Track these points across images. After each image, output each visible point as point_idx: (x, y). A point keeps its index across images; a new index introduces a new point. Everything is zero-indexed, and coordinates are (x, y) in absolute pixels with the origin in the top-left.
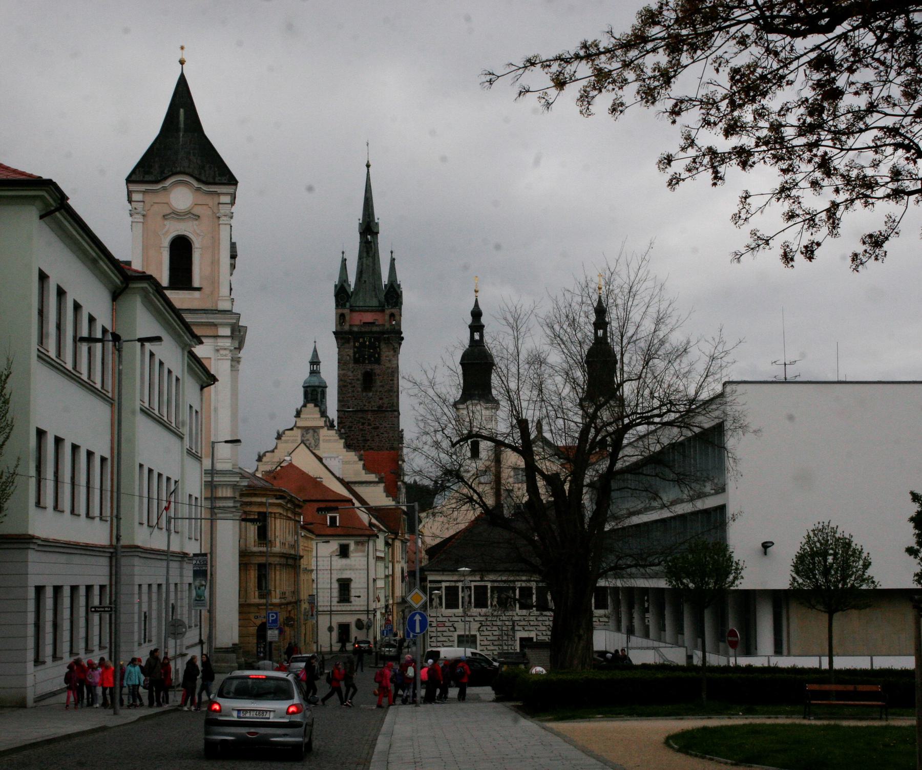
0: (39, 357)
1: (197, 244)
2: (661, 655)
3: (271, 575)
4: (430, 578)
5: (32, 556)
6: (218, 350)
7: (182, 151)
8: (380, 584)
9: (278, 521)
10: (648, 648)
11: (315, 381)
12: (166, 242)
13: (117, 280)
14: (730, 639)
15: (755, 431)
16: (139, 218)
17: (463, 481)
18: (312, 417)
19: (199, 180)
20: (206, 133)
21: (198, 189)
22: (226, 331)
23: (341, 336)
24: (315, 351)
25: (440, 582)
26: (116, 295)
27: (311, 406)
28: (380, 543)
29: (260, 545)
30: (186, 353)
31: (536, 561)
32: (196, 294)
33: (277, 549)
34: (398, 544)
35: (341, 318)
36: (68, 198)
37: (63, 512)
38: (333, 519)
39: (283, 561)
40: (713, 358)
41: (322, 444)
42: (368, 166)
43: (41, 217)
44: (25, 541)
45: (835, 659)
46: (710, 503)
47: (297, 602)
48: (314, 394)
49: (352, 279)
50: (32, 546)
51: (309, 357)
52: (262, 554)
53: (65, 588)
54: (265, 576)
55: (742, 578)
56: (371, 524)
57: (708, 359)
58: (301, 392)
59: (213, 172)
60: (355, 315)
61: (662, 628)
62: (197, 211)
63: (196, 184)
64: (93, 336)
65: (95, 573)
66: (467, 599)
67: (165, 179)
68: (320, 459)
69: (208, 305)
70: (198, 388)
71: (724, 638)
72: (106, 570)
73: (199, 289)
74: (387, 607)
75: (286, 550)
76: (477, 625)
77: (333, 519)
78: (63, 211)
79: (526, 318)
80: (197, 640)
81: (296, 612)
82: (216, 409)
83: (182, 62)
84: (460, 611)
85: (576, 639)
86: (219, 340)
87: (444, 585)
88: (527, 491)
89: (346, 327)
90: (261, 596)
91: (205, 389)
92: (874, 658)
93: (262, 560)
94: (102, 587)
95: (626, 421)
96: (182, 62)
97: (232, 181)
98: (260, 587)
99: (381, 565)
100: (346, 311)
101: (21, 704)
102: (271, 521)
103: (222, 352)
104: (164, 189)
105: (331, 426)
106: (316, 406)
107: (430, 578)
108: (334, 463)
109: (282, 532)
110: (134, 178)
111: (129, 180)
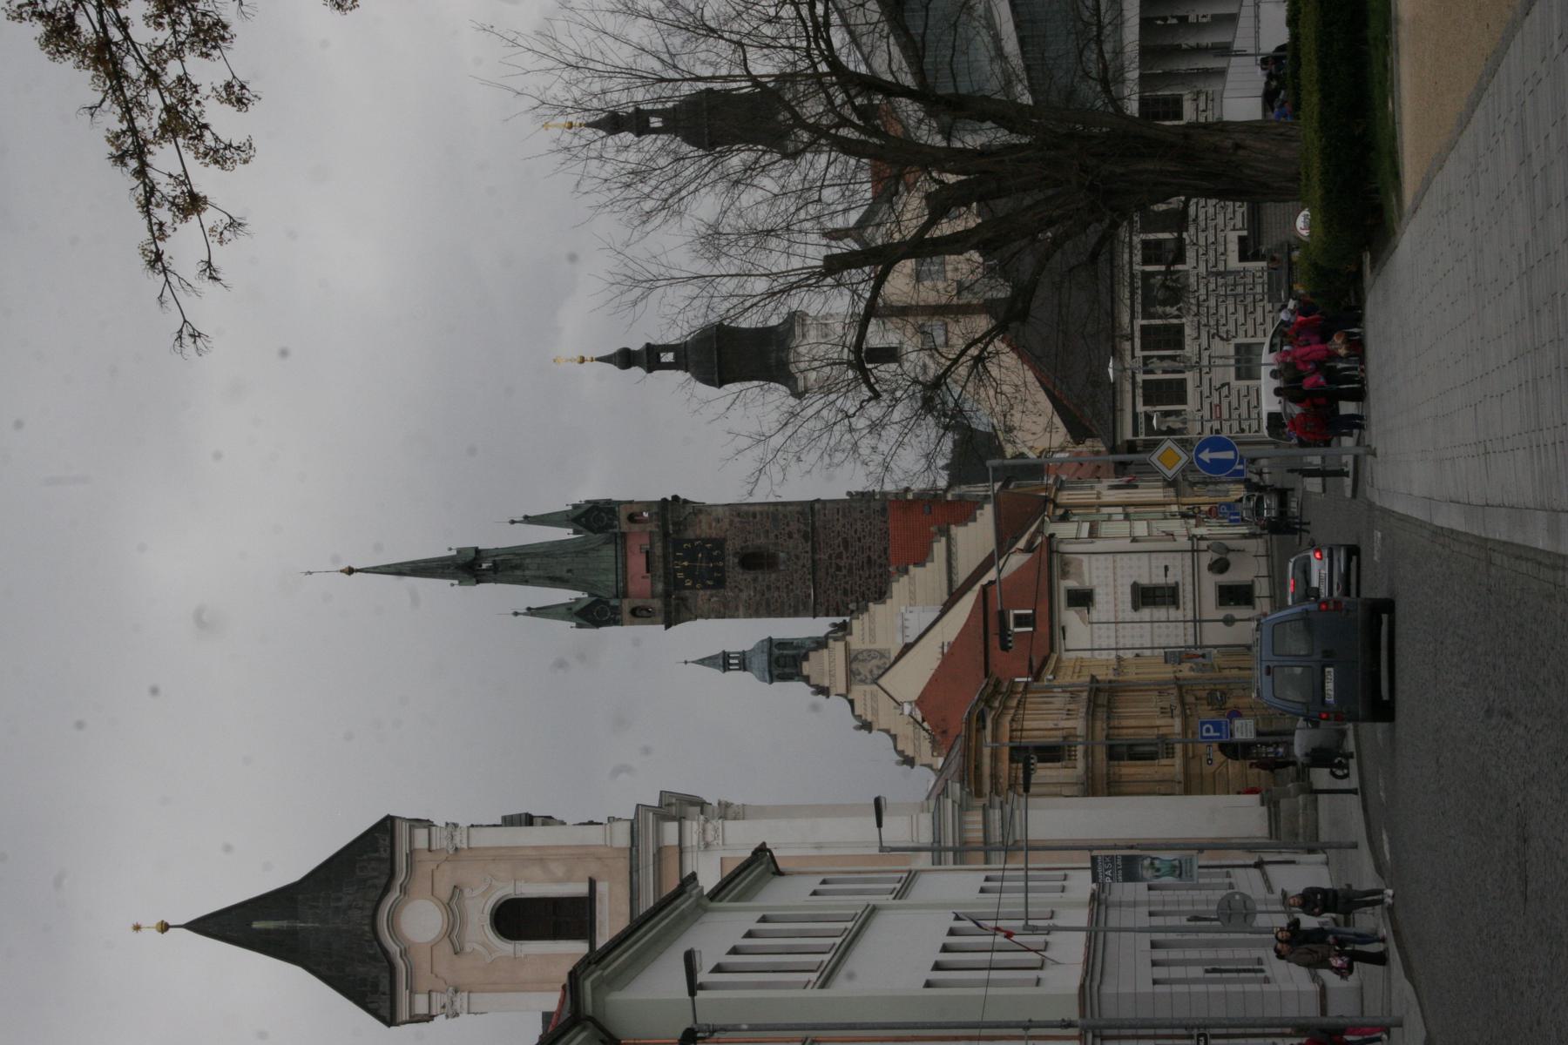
1: (507, 890)
4: (1129, 436)
6: (707, 845)
8: (1141, 529)
9: (1027, 725)
10: (1257, 16)
11: (761, 661)
12: (507, 947)
18: (829, 664)
19: (387, 889)
21: (404, 890)
22: (671, 829)
24: (702, 662)
25: (1135, 416)
27: (806, 668)
28: (1063, 530)
29: (1071, 757)
32: (602, 887)
33: (1078, 725)
34: (1065, 497)
35: (640, 614)
38: (1020, 621)
41: (879, 645)
42: (350, 571)
47: (1180, 685)
48: (784, 662)
49: (563, 596)
51: (715, 673)
56: (1029, 548)
59: (370, 863)
62: (444, 891)
63: (395, 894)
66: (1166, 364)
67: (385, 952)
68: (908, 647)
69: (623, 865)
70: (778, 879)
73: (592, 884)
74: (1184, 516)
77: (1020, 621)
79: (630, 264)
80: (1256, 872)
82: (819, 846)
83: (164, 927)
84: (1190, 377)
85: (1241, 152)
87: (1141, 408)
89: (657, 604)
90: (1170, 754)
91: (781, 866)
93: (1101, 754)
96: (164, 927)
97: (387, 826)
98: (1152, 756)
99: (1105, 529)
100: (626, 605)
104: (404, 953)
105: (844, 628)
106: (806, 657)
108: (916, 622)
109: (1048, 717)
110: (385, 1013)
111: (390, 1020)
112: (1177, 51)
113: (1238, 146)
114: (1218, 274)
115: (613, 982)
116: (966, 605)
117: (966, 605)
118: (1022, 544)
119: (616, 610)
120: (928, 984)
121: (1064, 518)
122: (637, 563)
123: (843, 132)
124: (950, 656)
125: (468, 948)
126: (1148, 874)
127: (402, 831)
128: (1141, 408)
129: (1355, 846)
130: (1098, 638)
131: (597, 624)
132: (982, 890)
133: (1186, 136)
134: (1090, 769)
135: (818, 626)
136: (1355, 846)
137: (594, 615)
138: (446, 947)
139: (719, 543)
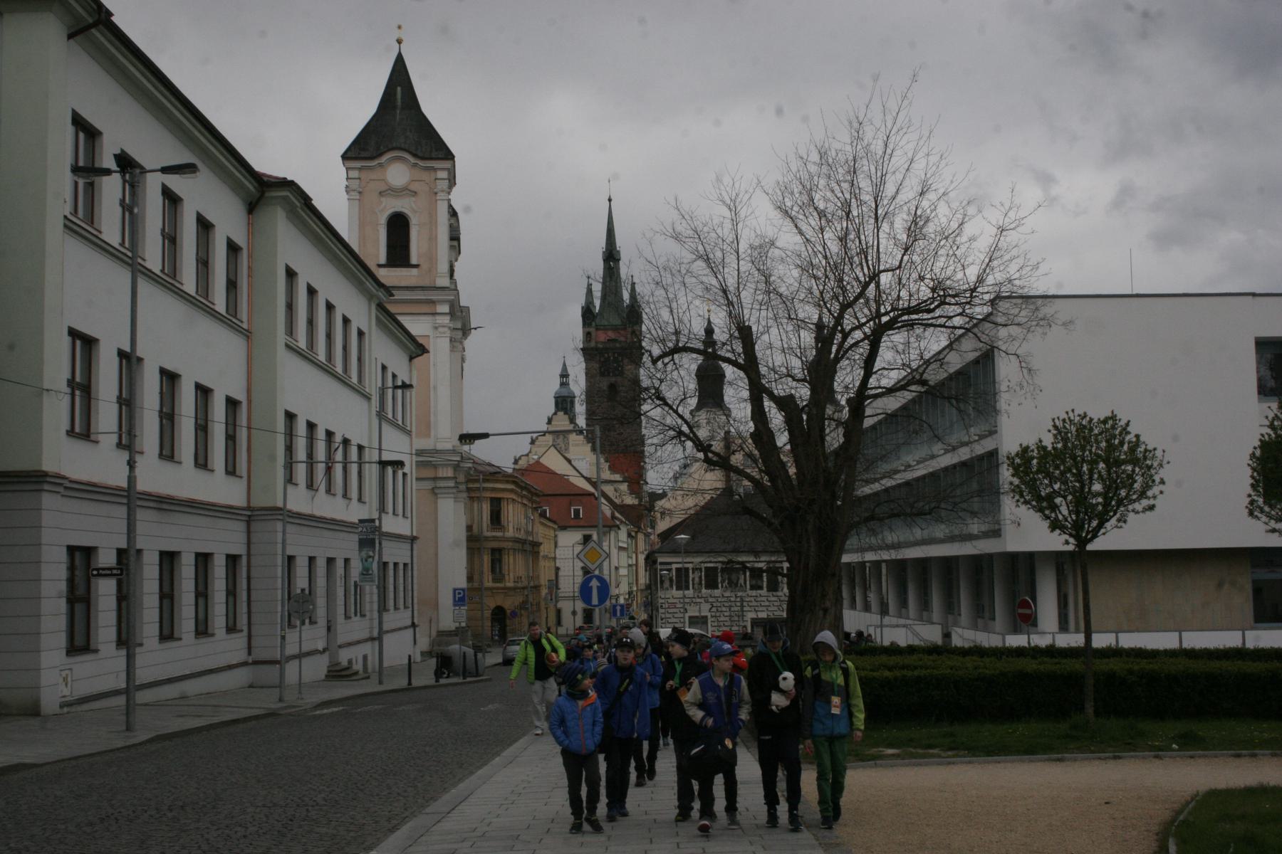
0: (65, 226)
1: (414, 221)
2: (916, 634)
3: (505, 558)
4: (660, 560)
5: (50, 501)
6: (436, 328)
7: (399, 129)
8: (623, 572)
9: (511, 507)
10: (897, 626)
11: (564, 392)
12: (383, 220)
13: (251, 187)
14: (1020, 611)
15: (1064, 324)
16: (355, 195)
17: (666, 404)
18: (562, 422)
19: (415, 155)
20: (424, 110)
21: (415, 165)
22: (446, 309)
23: (588, 353)
24: (564, 365)
25: (670, 563)
26: (252, 208)
27: (561, 413)
28: (623, 534)
29: (493, 530)
30: (374, 307)
31: (766, 513)
32: (414, 271)
33: (510, 533)
34: (641, 536)
35: (588, 335)
36: (111, 15)
37: (180, 463)
38: (577, 512)
39: (517, 546)
40: (1002, 230)
41: (571, 448)
42: (610, 200)
43: (70, 37)
44: (36, 479)
45: (1095, 636)
46: (980, 449)
47: (537, 588)
48: (564, 403)
49: (597, 303)
50: (46, 487)
51: (559, 371)
52: (495, 539)
53: (184, 555)
54: (500, 561)
55: (1162, 482)
56: (613, 517)
57: (994, 230)
58: (553, 401)
59: (430, 148)
60: (600, 333)
61: (903, 603)
62: (414, 187)
63: (412, 160)
64: (97, 165)
65: (224, 540)
66: (697, 580)
67: (381, 155)
68: (569, 461)
69: (426, 283)
70: (407, 359)
71: (982, 613)
72: (242, 538)
73: (417, 266)
74: (630, 593)
75: (522, 535)
76: (708, 606)
77: (577, 512)
78: (101, 27)
79: (747, 197)
80: (409, 623)
81: (536, 597)
82: (435, 388)
83: (399, 42)
84: (690, 593)
85: (821, 613)
86: (438, 317)
87: (674, 566)
88: (752, 419)
89: (593, 344)
90: (495, 580)
91: (416, 361)
92: (1184, 634)
93: (495, 545)
94: (232, 560)
95: (885, 319)
96: (399, 42)
97: (449, 156)
98: (493, 571)
99: (624, 555)
100: (592, 330)
101: (33, 711)
102: (504, 504)
103: (441, 330)
104: (380, 165)
105: (581, 432)
106: (566, 413)
107: (660, 560)
108: (580, 463)
109: (516, 517)
110: (349, 155)
111: (345, 157)
112: (865, 589)
113: (826, 611)
114: (742, 606)
115: (293, 215)
116: (590, 489)
117: (590, 489)
118: (617, 515)
119: (590, 325)
120: (290, 417)
121: (629, 535)
122: (611, 335)
123: (839, 336)
124: (562, 478)
125: (383, 199)
126: (364, 554)
127: (447, 164)
128: (674, 566)
129: (381, 683)
130: (566, 548)
131: (584, 316)
132: (290, 417)
133: (834, 575)
134: (487, 538)
135: (581, 421)
136: (381, 683)
137: (588, 314)
138: (384, 188)
139: (621, 373)
